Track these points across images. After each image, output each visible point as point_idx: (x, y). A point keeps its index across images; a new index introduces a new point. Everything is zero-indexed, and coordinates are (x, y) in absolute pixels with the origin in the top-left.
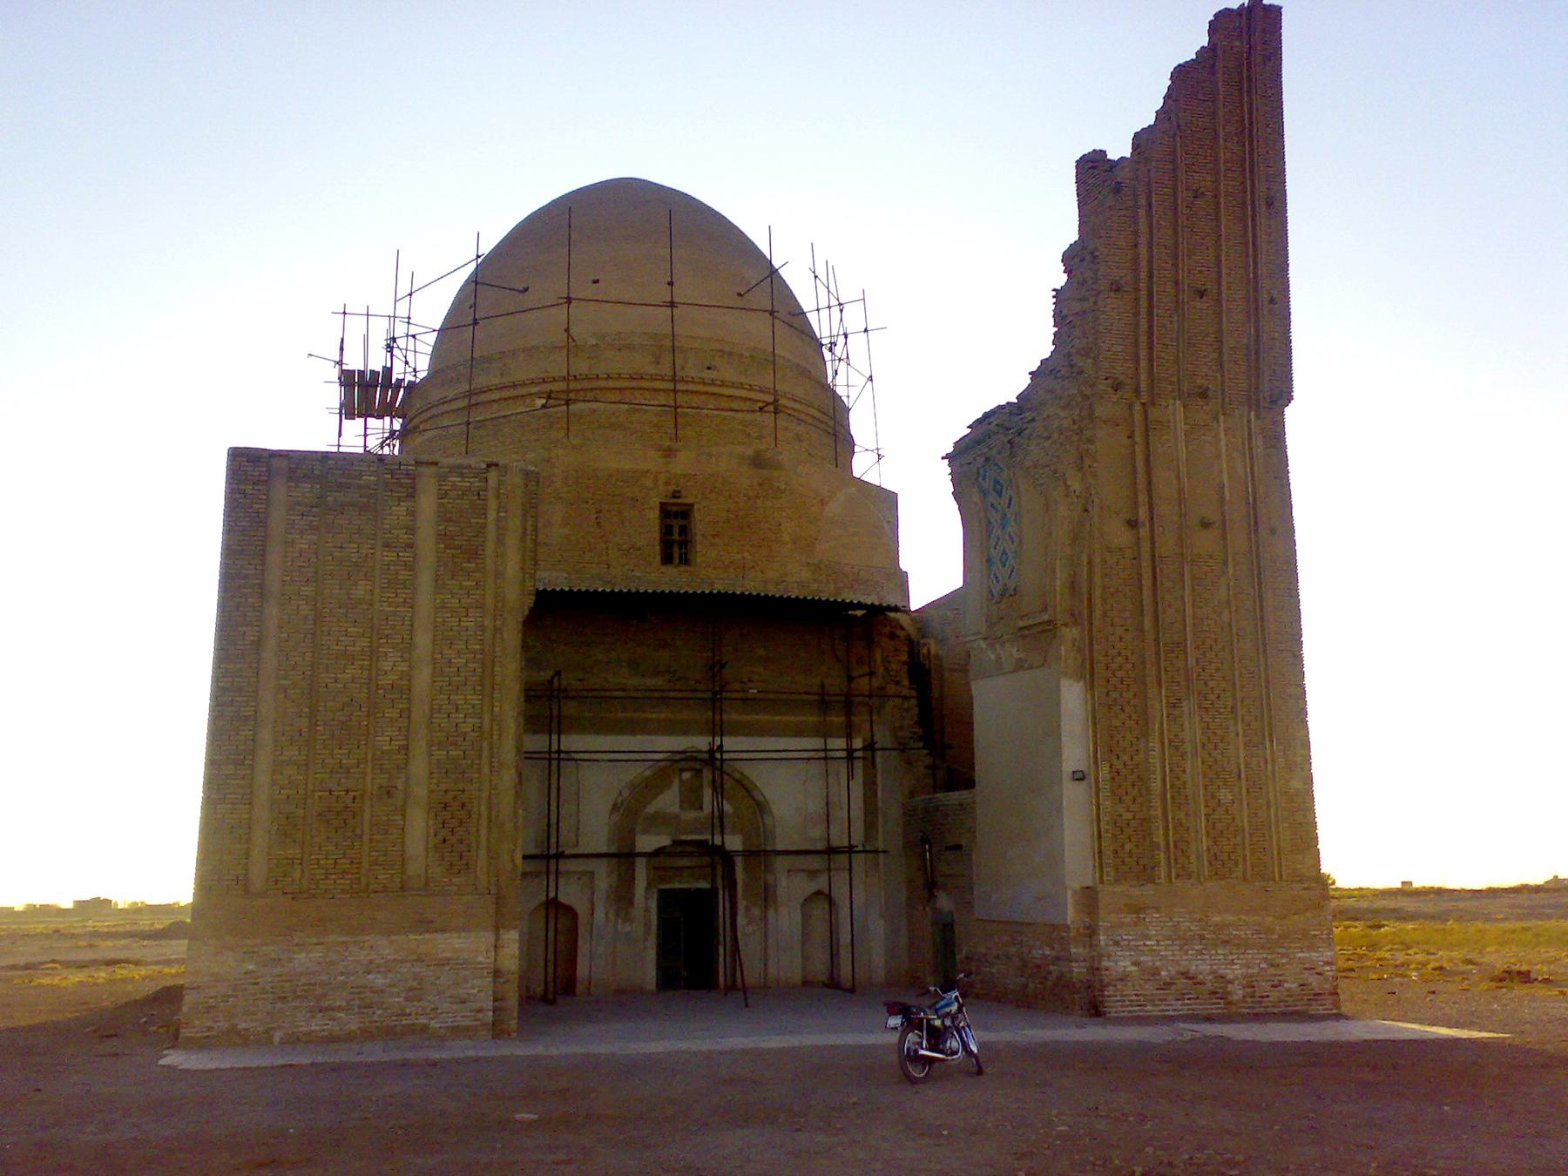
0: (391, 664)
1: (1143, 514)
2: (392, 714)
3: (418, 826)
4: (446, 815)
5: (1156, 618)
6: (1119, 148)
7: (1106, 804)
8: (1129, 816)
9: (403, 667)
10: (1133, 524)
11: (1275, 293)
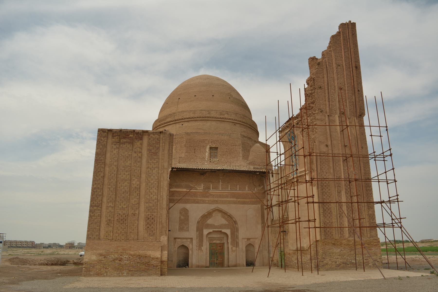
0: (135, 182)
1: (329, 143)
2: (135, 194)
3: (142, 223)
4: (148, 221)
5: (334, 170)
6: (352, 22)
7: (322, 218)
8: (328, 221)
9: (138, 183)
10: (327, 146)
11: (359, 89)
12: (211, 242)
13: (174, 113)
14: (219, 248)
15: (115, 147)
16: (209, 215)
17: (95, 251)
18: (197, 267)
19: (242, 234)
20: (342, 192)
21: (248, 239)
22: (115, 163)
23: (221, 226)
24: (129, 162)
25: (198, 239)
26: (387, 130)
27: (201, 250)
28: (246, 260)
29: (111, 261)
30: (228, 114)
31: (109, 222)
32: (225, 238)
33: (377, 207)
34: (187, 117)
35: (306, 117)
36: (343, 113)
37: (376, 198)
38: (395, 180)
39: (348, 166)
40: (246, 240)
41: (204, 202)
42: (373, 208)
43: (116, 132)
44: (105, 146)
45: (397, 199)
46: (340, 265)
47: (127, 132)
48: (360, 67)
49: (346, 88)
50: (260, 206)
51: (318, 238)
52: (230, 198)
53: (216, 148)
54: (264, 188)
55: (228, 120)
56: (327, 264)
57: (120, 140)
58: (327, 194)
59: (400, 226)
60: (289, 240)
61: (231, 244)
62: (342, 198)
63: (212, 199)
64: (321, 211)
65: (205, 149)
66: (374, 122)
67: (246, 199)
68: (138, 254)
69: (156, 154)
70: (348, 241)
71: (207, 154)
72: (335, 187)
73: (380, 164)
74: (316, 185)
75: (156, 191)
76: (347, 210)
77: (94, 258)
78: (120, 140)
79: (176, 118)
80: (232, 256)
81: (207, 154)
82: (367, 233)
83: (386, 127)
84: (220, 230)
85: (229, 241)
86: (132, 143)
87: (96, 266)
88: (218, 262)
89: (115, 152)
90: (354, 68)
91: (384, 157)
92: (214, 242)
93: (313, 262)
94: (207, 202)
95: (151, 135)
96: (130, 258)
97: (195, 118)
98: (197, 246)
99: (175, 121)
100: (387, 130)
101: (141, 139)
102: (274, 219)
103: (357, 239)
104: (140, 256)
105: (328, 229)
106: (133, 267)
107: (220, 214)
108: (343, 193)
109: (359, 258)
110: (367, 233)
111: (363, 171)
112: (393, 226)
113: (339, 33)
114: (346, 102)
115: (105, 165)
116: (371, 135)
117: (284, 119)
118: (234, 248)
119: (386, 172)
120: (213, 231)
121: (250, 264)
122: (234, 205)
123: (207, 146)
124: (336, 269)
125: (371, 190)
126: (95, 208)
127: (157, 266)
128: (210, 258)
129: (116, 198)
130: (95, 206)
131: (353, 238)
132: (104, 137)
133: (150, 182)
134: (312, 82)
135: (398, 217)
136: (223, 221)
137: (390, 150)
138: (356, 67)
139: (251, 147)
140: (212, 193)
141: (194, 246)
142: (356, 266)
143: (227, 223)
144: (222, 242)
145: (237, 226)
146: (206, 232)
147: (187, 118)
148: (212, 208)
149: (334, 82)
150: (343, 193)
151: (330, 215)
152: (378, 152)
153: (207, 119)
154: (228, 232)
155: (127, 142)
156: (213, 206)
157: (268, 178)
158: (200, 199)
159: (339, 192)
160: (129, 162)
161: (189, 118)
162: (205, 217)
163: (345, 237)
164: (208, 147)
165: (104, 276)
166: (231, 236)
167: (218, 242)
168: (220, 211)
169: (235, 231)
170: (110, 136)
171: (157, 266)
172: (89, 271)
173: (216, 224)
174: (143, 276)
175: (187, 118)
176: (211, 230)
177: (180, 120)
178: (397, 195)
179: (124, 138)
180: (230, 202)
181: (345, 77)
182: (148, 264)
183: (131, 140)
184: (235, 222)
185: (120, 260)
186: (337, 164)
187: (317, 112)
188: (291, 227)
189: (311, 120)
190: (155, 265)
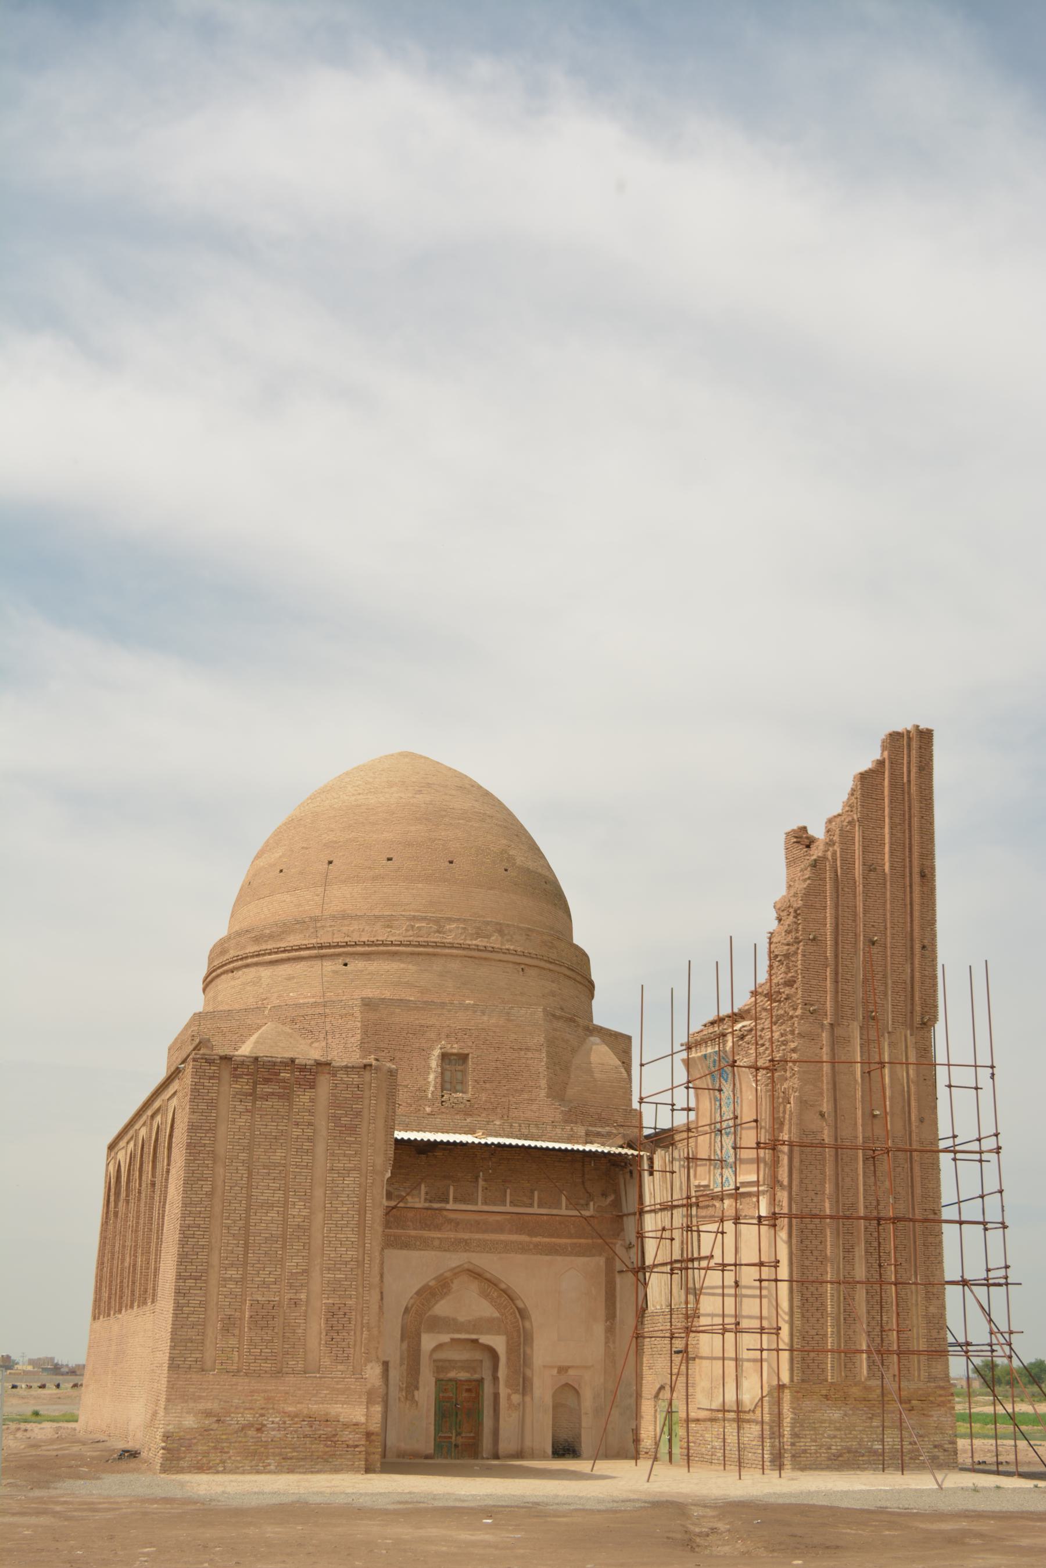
0: (297, 1210)
3: (316, 1327)
12: (441, 1376)
13: (315, 919)
14: (465, 1395)
15: (240, 1108)
16: (440, 1288)
17: (191, 1405)
18: (398, 1456)
19: (546, 1352)
20: (856, 1249)
21: (562, 1370)
22: (243, 1156)
23: (477, 1325)
24: (280, 1153)
25: (405, 1367)
26: (993, 1074)
27: (414, 1402)
28: (553, 1436)
29: (236, 1432)
30: (500, 932)
31: (229, 1325)
32: (487, 1364)
33: (953, 1295)
34: (364, 939)
35: (767, 1024)
36: (871, 1018)
37: (951, 1272)
38: (1003, 1223)
39: (879, 1174)
40: (555, 1372)
41: (425, 1244)
42: (941, 1297)
43: (243, 1063)
44: (212, 1104)
45: (1006, 1278)
46: (841, 1455)
47: (274, 1064)
48: (933, 875)
49: (889, 940)
50: (601, 1261)
51: (785, 1378)
52: (510, 1232)
53: (463, 1058)
54: (617, 1204)
55: (501, 956)
56: (805, 1451)
57: (254, 1088)
58: (815, 1253)
59: (1008, 1353)
60: (697, 1378)
61: (507, 1386)
62: (857, 1266)
63: (452, 1235)
64: (797, 1302)
65: (427, 1058)
66: (961, 1053)
67: (558, 1237)
68: (305, 1412)
69: (352, 1129)
70: (867, 1389)
71: (431, 1077)
72: (838, 1234)
73: (969, 1170)
74: (786, 1228)
75: (353, 1238)
76: (868, 1302)
77: (190, 1422)
78: (254, 1088)
79: (325, 939)
80: (508, 1422)
81: (431, 1077)
82: (919, 1370)
83: (992, 1067)
84: (474, 1337)
85: (502, 1372)
86: (287, 1096)
87: (195, 1444)
88: (460, 1441)
89: (241, 1122)
90: (916, 878)
91: (981, 1152)
92: (452, 1374)
93: (767, 1444)
94: (436, 1243)
95: (341, 1075)
96: (284, 1423)
97: (392, 944)
98: (401, 1390)
99: (321, 947)
100: (993, 1074)
101: (312, 1086)
102: (651, 1308)
103: (891, 1385)
104: (311, 1419)
105: (812, 1354)
106: (294, 1449)
107: (474, 1286)
108: (860, 1251)
109: (891, 1439)
110: (919, 1370)
111: (918, 1191)
112: (993, 1351)
113: (881, 763)
114: (886, 985)
115: (214, 1162)
116: (950, 1086)
117: (704, 1014)
118: (516, 1398)
119: (982, 1197)
120: (452, 1340)
121: (565, 1449)
122: (520, 1258)
123: (432, 1048)
124: (828, 1468)
125: (940, 1244)
126: (190, 1283)
127: (357, 1446)
128: (438, 1428)
129: (246, 1254)
130: (190, 1277)
131: (879, 1382)
132: (211, 1078)
133: (336, 1212)
134: (791, 917)
135: (1004, 1328)
136: (486, 1309)
137: (996, 1135)
138: (923, 876)
139: (574, 1051)
140: (452, 1216)
141: (391, 1388)
142: (881, 1461)
143: (496, 1314)
144: (476, 1376)
145: (527, 1324)
146: (428, 1342)
147: (364, 944)
148: (454, 1264)
149: (855, 921)
150: (860, 1251)
151: (818, 1315)
152: (966, 1132)
153: (431, 950)
154: (498, 1343)
155: (273, 1094)
156: (455, 1259)
157: (635, 1174)
158: (413, 1233)
159: (849, 1250)
160: (280, 1153)
161: (373, 944)
162: (430, 1294)
163: (858, 1379)
164: (437, 1052)
165: (218, 1472)
166: (508, 1359)
167: (463, 1375)
168: (476, 1274)
169: (521, 1340)
170: (226, 1075)
171: (357, 1446)
172: (179, 1459)
173: (461, 1319)
174: (319, 1472)
175: (364, 944)
176: (445, 1338)
177: (338, 946)
178: (1007, 1267)
179: (267, 1081)
180: (508, 1248)
181: (888, 906)
182: (331, 1439)
183: (284, 1088)
184: (523, 1314)
185: (258, 1430)
186: (847, 1169)
187: (799, 1012)
188: (706, 1344)
189: (782, 1035)
190: (351, 1443)
